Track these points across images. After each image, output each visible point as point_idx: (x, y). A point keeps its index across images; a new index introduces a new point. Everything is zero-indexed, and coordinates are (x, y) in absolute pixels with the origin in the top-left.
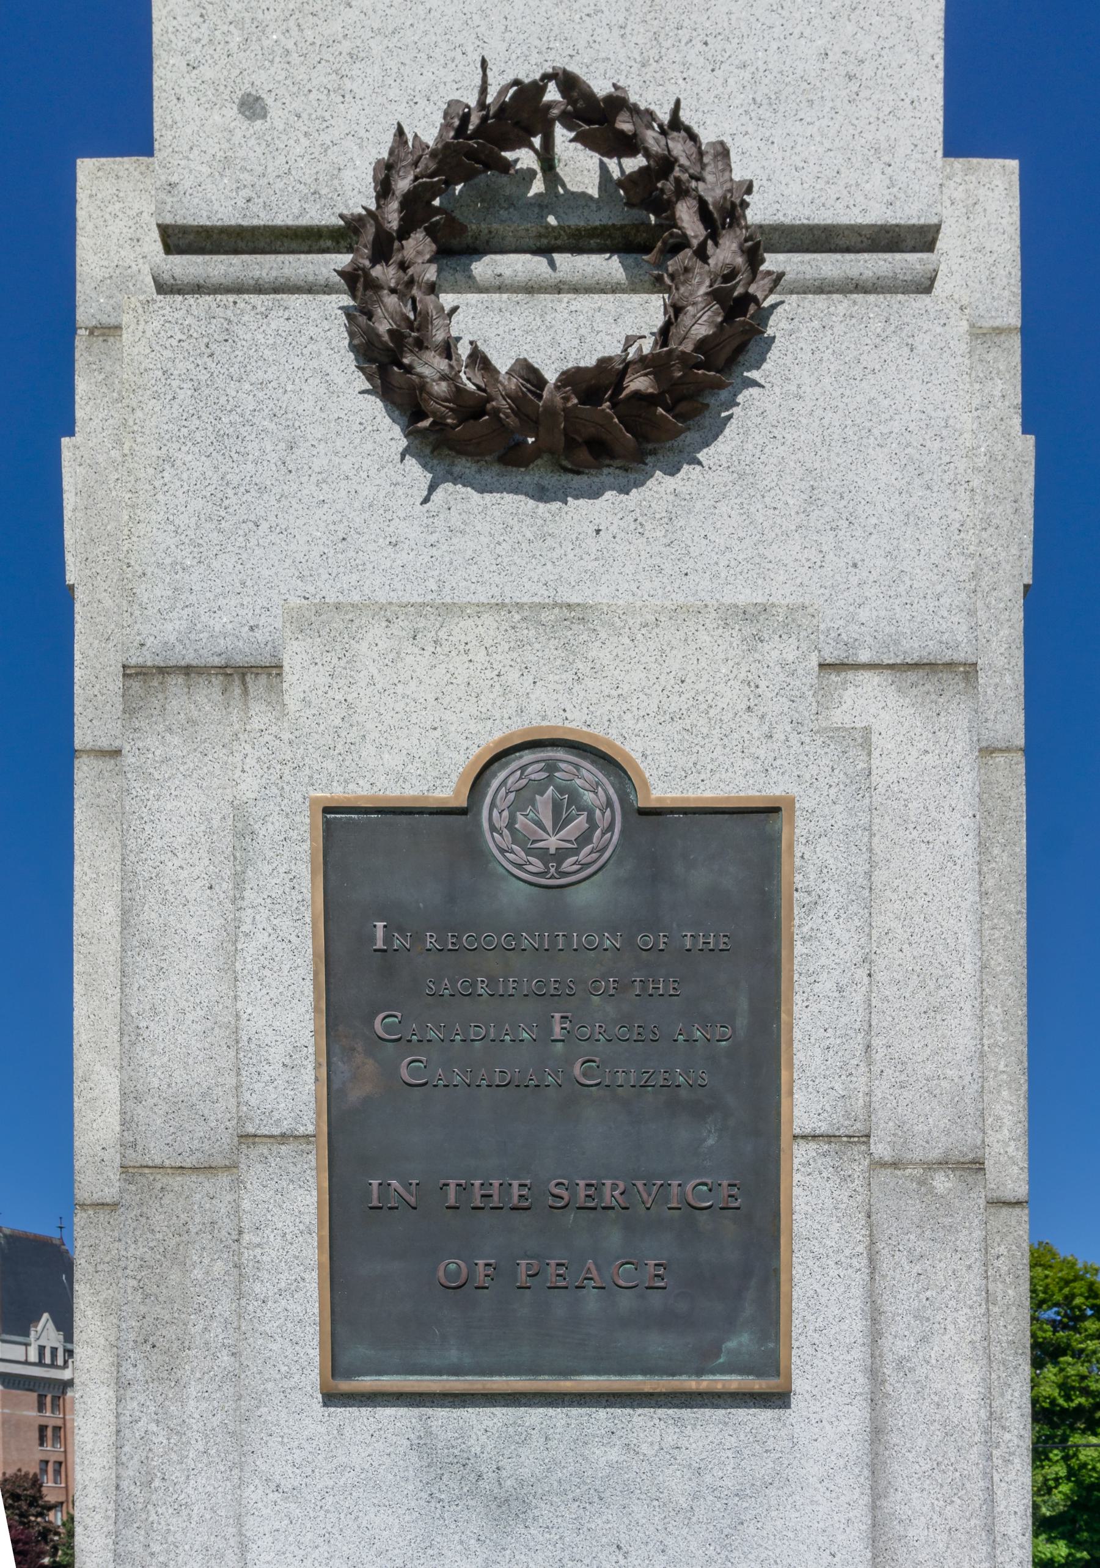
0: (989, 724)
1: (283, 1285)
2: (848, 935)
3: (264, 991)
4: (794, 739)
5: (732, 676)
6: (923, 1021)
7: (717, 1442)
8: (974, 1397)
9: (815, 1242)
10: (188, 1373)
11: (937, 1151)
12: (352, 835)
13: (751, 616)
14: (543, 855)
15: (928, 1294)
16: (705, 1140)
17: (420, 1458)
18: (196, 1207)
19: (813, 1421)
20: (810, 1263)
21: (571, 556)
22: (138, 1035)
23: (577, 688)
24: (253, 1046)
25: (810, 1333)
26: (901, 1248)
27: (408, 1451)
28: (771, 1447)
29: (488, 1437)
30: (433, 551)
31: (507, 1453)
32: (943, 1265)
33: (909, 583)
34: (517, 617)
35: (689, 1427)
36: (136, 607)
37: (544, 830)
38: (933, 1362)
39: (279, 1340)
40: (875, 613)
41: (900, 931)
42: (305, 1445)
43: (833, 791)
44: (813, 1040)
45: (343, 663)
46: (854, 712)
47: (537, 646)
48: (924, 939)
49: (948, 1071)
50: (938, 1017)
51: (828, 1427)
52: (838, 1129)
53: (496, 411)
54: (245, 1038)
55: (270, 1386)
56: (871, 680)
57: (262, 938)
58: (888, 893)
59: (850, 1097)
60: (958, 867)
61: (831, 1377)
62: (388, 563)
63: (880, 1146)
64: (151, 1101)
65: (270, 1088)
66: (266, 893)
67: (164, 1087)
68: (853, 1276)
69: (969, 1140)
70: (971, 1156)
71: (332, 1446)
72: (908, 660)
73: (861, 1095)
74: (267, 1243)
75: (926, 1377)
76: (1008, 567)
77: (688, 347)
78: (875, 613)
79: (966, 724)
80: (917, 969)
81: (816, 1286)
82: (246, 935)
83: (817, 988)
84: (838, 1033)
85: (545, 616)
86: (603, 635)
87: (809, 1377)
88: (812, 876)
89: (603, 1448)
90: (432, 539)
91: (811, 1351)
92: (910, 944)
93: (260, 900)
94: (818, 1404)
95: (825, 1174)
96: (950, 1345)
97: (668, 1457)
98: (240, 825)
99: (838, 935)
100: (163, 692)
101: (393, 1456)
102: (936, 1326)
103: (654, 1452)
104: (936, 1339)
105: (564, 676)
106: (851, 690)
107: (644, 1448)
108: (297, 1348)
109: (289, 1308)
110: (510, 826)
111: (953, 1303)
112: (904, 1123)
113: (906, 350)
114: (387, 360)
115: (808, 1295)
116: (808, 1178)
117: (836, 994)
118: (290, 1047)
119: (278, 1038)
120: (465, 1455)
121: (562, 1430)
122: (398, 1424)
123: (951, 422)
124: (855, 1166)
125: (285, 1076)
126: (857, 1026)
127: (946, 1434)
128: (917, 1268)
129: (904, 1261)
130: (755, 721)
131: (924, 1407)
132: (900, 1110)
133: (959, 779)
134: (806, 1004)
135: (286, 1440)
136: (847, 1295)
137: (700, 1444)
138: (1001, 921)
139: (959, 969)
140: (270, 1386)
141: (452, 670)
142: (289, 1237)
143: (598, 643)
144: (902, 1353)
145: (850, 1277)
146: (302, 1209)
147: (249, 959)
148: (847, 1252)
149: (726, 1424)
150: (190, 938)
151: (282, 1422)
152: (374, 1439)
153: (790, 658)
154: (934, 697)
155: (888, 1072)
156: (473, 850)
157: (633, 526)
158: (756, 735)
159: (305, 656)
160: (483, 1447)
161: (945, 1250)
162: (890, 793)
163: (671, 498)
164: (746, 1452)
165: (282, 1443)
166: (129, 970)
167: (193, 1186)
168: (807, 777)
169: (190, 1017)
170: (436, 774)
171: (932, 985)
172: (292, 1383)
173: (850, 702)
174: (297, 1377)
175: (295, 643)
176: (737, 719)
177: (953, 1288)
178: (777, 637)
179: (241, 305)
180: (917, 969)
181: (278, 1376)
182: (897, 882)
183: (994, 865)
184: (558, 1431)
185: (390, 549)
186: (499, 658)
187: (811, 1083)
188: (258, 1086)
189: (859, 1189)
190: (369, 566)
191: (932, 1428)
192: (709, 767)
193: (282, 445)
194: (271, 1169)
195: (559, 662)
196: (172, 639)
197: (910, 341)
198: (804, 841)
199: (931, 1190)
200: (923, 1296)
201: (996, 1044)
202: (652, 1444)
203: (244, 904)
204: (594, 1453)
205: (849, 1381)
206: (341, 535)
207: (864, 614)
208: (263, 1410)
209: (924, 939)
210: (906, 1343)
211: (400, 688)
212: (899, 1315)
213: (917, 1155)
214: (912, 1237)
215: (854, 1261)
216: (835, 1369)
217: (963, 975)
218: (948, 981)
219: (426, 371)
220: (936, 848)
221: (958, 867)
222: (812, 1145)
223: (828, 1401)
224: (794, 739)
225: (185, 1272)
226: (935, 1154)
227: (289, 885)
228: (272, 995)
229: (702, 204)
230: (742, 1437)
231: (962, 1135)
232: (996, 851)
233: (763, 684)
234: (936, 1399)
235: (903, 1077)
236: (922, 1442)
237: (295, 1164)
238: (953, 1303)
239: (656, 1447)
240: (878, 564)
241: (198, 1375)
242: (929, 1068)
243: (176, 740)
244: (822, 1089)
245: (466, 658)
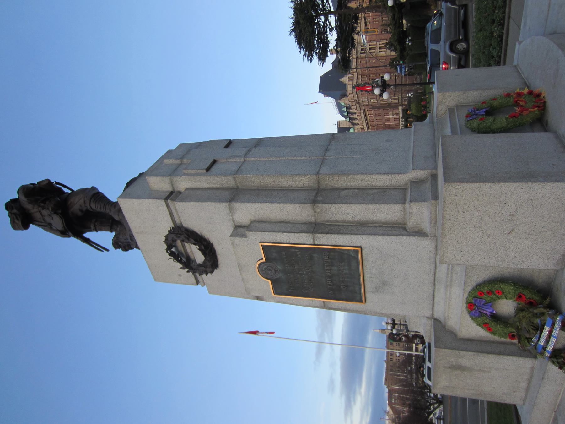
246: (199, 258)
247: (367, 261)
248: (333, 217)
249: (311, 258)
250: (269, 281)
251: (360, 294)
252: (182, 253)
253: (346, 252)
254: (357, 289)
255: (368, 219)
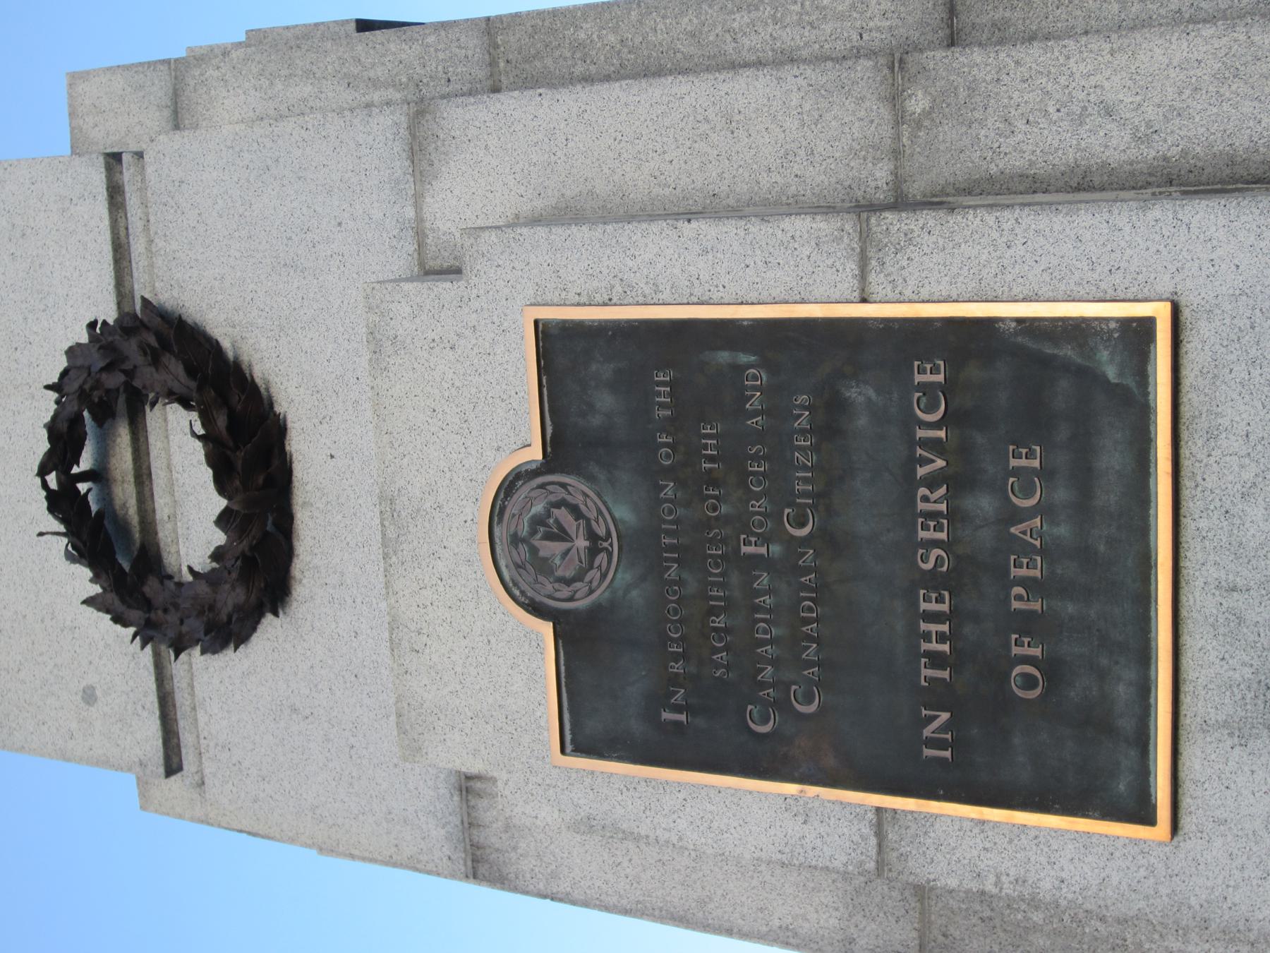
0: (470, 53)
1: (1043, 860)
2: (650, 245)
3: (733, 831)
4: (475, 304)
5: (426, 364)
6: (741, 133)
7: (1240, 388)
8: (1186, 44)
9: (984, 273)
10: (1153, 946)
11: (882, 110)
12: (583, 738)
13: (376, 342)
14: (593, 551)
15: (1051, 110)
16: (869, 399)
17: (1258, 737)
18: (964, 906)
19: (1212, 269)
20: (1009, 278)
21: (352, 482)
22: (787, 928)
23: (446, 509)
24: (787, 850)
25: (1096, 276)
26: (996, 145)
27: (1248, 751)
28: (1248, 322)
29: (1231, 657)
30: (359, 600)
31: (1252, 638)
32: (1016, 95)
33: (350, 174)
34: (394, 559)
35: (1220, 421)
36: (421, 857)
37: (569, 550)
38: (1138, 98)
39: (1108, 871)
40: (376, 204)
41: (652, 164)
42: (1239, 862)
43: (516, 264)
44: (758, 280)
45: (442, 717)
46: (457, 220)
47: (415, 543)
48: (659, 139)
49: (793, 104)
50: (737, 117)
51: (1220, 252)
52: (853, 249)
53: (252, 548)
54: (779, 856)
55: (1164, 890)
56: (432, 205)
57: (682, 824)
58: (616, 178)
59: (818, 237)
60: (588, 108)
61: (1153, 250)
62: (370, 641)
63: (878, 174)
64: (853, 930)
65: (829, 840)
66: (641, 814)
67: (838, 914)
68: (1024, 226)
69: (868, 74)
70: (886, 71)
71: (1240, 833)
72: (410, 170)
73: (814, 226)
74: (995, 868)
75: (1159, 106)
76: (341, 49)
77: (193, 385)
78: (376, 204)
79: (460, 110)
80: (688, 143)
81: (1038, 269)
82: (680, 839)
83: (705, 276)
84: (749, 252)
85: (391, 533)
86: (402, 483)
87: (1153, 276)
88: (596, 284)
89: (1247, 525)
90: (349, 601)
91: (1120, 274)
92: (664, 153)
93: (648, 821)
94: (1188, 265)
95: (905, 263)
96: (1116, 79)
97: (1259, 447)
98: (583, 828)
99: (651, 256)
100: (484, 848)
101: (1254, 768)
102: (1092, 98)
103: (1253, 465)
104: (1110, 97)
105: (438, 520)
106: (439, 223)
107: (1248, 475)
108: (1117, 854)
109: (1069, 856)
110: (568, 582)
111: (1063, 80)
112: (851, 149)
113: (184, 186)
114: (228, 631)
115: (1048, 279)
116: (909, 282)
117: (710, 256)
118: (786, 815)
119: (778, 824)
120: (1255, 686)
121: (1223, 572)
122: (1213, 757)
123: (229, 144)
124: (894, 229)
125: (816, 824)
126: (742, 233)
127: (1235, 77)
128: (1020, 125)
129: (1012, 141)
130: (462, 342)
131: (1199, 107)
132: (837, 155)
133: (508, 113)
134: (721, 288)
135: (1232, 883)
136: (1047, 233)
137: (1242, 408)
138: (649, 23)
139: (687, 98)
140: (1164, 890)
141: (440, 621)
142: (988, 845)
143: (409, 487)
144: (1127, 138)
145: (1025, 230)
146: (956, 828)
147: (703, 840)
148: (995, 235)
149: (1215, 376)
150: (693, 864)
151: (1209, 884)
152: (1232, 786)
153: (408, 309)
154: (439, 143)
155: (796, 169)
156: (595, 615)
157: (325, 425)
158: (474, 341)
159: (440, 749)
160: (1244, 664)
161: (997, 94)
162: (524, 181)
163: (301, 390)
164: (1253, 352)
165: (1236, 887)
166: (727, 925)
167: (940, 905)
168: (506, 291)
169: (768, 878)
170: (527, 646)
171: (704, 127)
172: (1160, 866)
173: (449, 224)
174: (1152, 860)
175: (430, 756)
176: (462, 359)
177: (1044, 80)
178: (392, 323)
179: (206, 734)
180: (688, 143)
181: (1152, 880)
182: (606, 170)
183: (595, 36)
184: (1224, 577)
185: (360, 638)
186: (427, 579)
187: (804, 281)
188: (828, 851)
189: (921, 222)
190: (374, 657)
191: (1227, 94)
192: (504, 387)
193: (294, 716)
194: (914, 852)
195: (427, 524)
196: (443, 832)
197: (177, 184)
198: (564, 293)
199: (927, 114)
200: (1055, 116)
201: (774, 16)
202: (1242, 466)
203: (652, 836)
204: (1254, 536)
205: (1157, 228)
206: (353, 678)
207: (377, 214)
208: (1193, 901)
209: (659, 139)
210: (1114, 134)
211: (459, 669)
212: (1079, 144)
213: (887, 131)
214: (983, 132)
215: (1006, 226)
216: (1143, 245)
217: (693, 94)
218: (700, 110)
219: (230, 604)
220: (571, 131)
221: (588, 108)
222: (872, 277)
223: (1184, 253)
224: (475, 304)
225: (1035, 928)
226: (885, 112)
227: (632, 792)
228: (736, 824)
229: (102, 369)
230: (1233, 357)
231: (862, 83)
232: (582, 36)
233: (431, 335)
234: (1187, 92)
235: (802, 153)
236: (1247, 106)
237: (907, 828)
238: (1063, 80)
239: (1247, 461)
240: (337, 203)
241: (1156, 936)
242: (791, 124)
243: (522, 845)
244: (811, 269)
245: (430, 608)
246: (191, 518)
247: (1212, 436)
248: (1008, 144)
249: (831, 419)
250: (546, 629)
251: (1143, 741)
252: (123, 527)
253: (1067, 352)
254: (1123, 692)
255: (1241, 142)
